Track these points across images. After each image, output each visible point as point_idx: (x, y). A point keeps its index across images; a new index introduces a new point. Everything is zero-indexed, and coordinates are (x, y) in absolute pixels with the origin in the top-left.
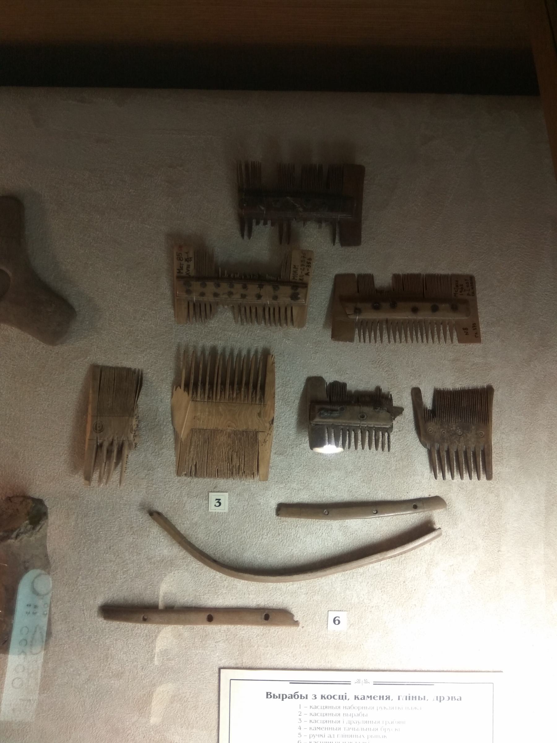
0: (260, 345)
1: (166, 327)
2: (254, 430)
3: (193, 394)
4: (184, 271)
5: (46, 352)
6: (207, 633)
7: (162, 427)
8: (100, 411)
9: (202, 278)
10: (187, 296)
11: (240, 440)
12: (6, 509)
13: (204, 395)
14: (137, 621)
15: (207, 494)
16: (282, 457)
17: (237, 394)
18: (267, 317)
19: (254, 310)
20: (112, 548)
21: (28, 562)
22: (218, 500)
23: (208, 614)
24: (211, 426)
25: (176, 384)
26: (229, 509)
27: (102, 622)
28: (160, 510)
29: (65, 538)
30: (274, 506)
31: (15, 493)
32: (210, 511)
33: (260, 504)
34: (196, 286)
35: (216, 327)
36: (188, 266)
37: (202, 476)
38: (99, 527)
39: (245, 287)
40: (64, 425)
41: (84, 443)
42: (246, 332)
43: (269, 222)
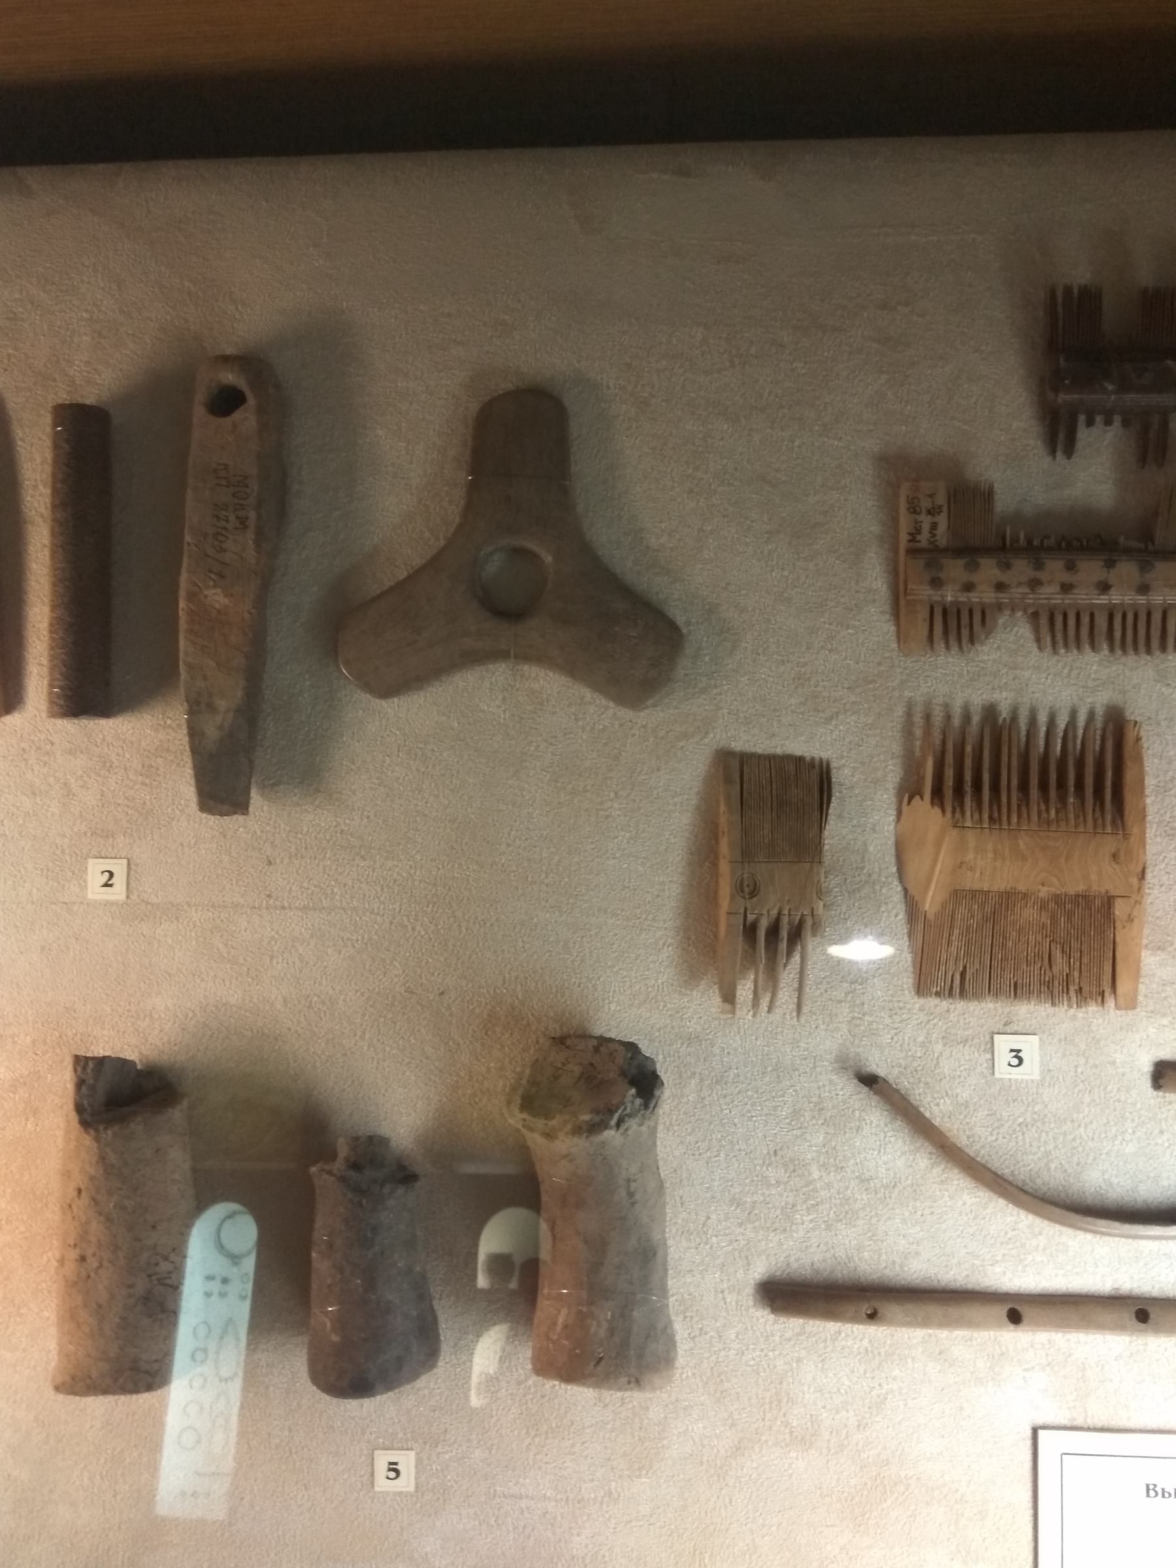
0: (1101, 699)
1: (880, 664)
2: (1103, 891)
3: (954, 812)
4: (924, 538)
5: (621, 725)
6: (1004, 1349)
7: (877, 888)
8: (746, 853)
9: (968, 551)
10: (932, 592)
11: (1070, 915)
12: (564, 1064)
13: (980, 814)
14: (855, 1320)
15: (988, 1038)
16: (1162, 955)
17: (1057, 812)
18: (1118, 634)
19: (1085, 620)
20: (780, 1153)
21: (635, 1181)
22: (1017, 1053)
23: (1010, 1306)
24: (1001, 883)
25: (909, 791)
26: (1042, 1072)
27: (764, 1318)
28: (881, 1072)
29: (676, 1128)
30: (1147, 1068)
31: (565, 1029)
32: (997, 1075)
33: (1114, 1063)
34: (955, 569)
35: (994, 661)
36: (934, 526)
37: (977, 996)
38: (748, 1106)
39: (1071, 567)
40: (663, 882)
41: (716, 925)
42: (1066, 671)
43: (1117, 419)
